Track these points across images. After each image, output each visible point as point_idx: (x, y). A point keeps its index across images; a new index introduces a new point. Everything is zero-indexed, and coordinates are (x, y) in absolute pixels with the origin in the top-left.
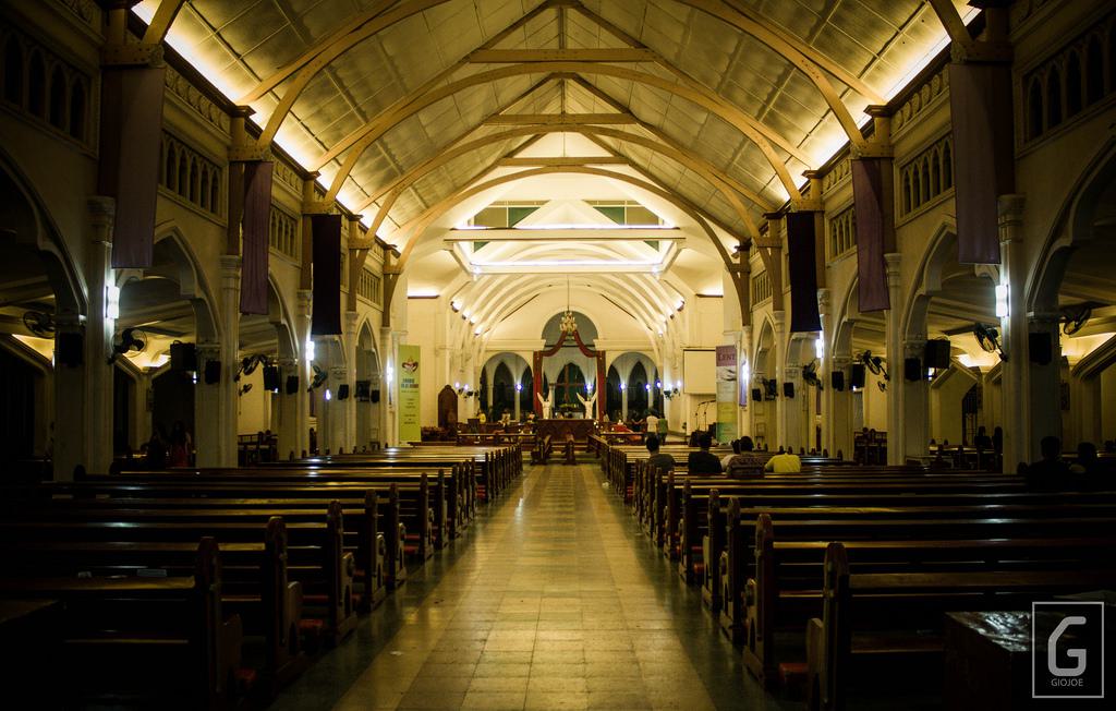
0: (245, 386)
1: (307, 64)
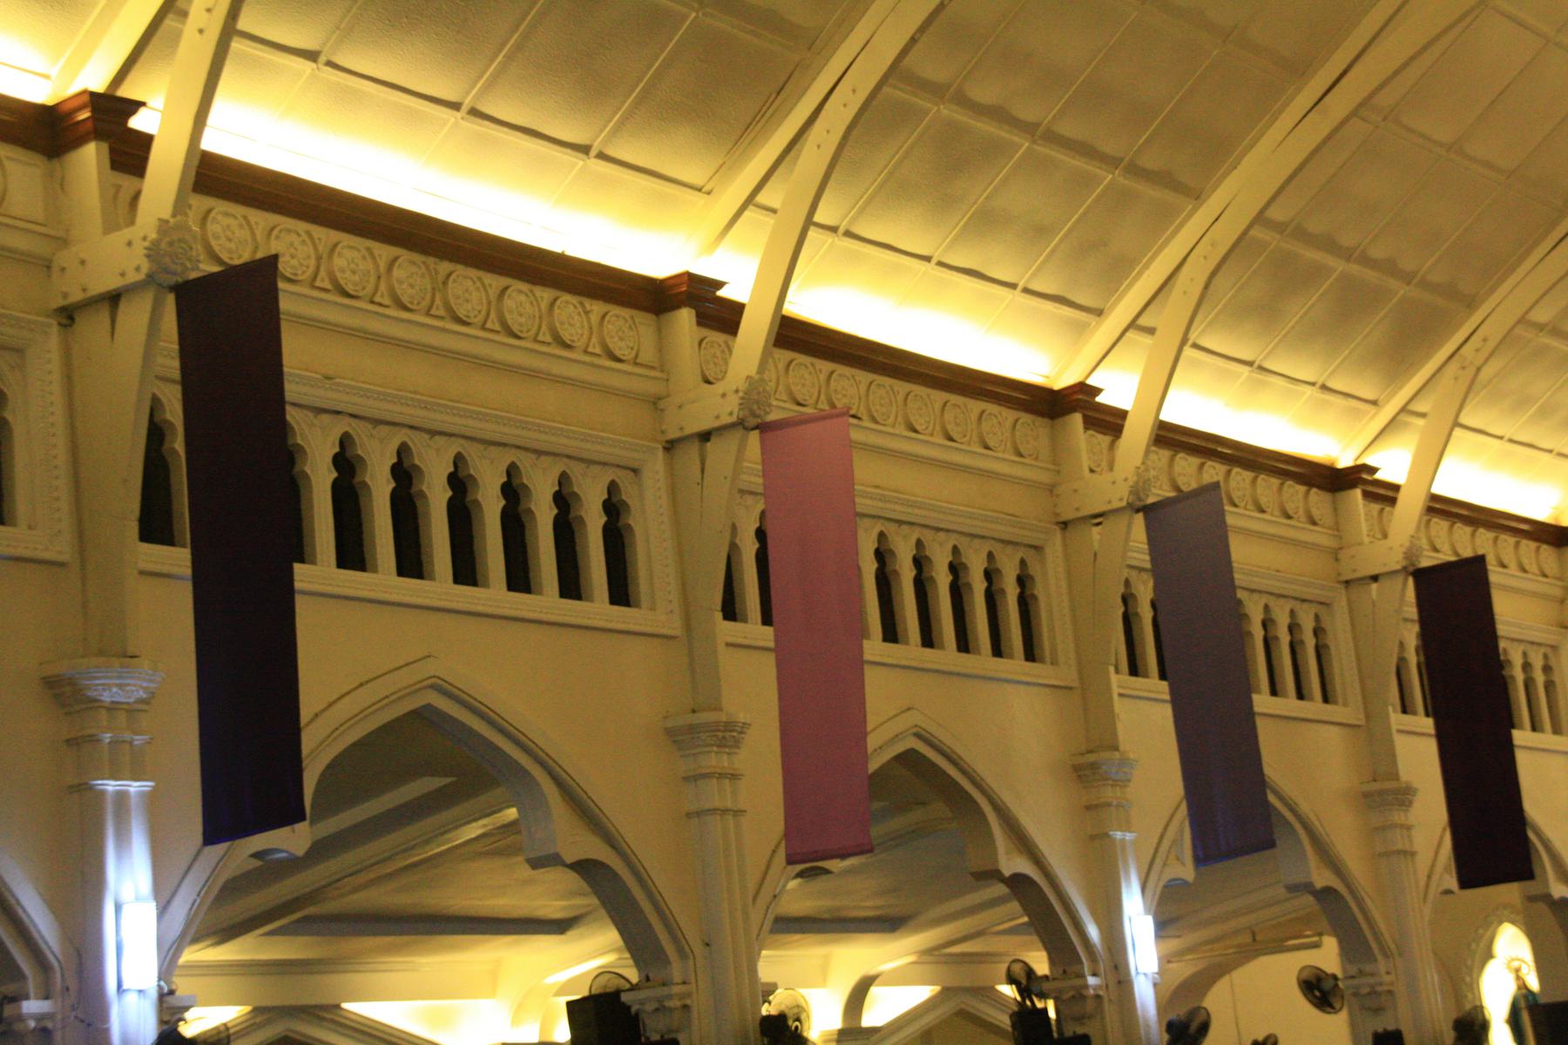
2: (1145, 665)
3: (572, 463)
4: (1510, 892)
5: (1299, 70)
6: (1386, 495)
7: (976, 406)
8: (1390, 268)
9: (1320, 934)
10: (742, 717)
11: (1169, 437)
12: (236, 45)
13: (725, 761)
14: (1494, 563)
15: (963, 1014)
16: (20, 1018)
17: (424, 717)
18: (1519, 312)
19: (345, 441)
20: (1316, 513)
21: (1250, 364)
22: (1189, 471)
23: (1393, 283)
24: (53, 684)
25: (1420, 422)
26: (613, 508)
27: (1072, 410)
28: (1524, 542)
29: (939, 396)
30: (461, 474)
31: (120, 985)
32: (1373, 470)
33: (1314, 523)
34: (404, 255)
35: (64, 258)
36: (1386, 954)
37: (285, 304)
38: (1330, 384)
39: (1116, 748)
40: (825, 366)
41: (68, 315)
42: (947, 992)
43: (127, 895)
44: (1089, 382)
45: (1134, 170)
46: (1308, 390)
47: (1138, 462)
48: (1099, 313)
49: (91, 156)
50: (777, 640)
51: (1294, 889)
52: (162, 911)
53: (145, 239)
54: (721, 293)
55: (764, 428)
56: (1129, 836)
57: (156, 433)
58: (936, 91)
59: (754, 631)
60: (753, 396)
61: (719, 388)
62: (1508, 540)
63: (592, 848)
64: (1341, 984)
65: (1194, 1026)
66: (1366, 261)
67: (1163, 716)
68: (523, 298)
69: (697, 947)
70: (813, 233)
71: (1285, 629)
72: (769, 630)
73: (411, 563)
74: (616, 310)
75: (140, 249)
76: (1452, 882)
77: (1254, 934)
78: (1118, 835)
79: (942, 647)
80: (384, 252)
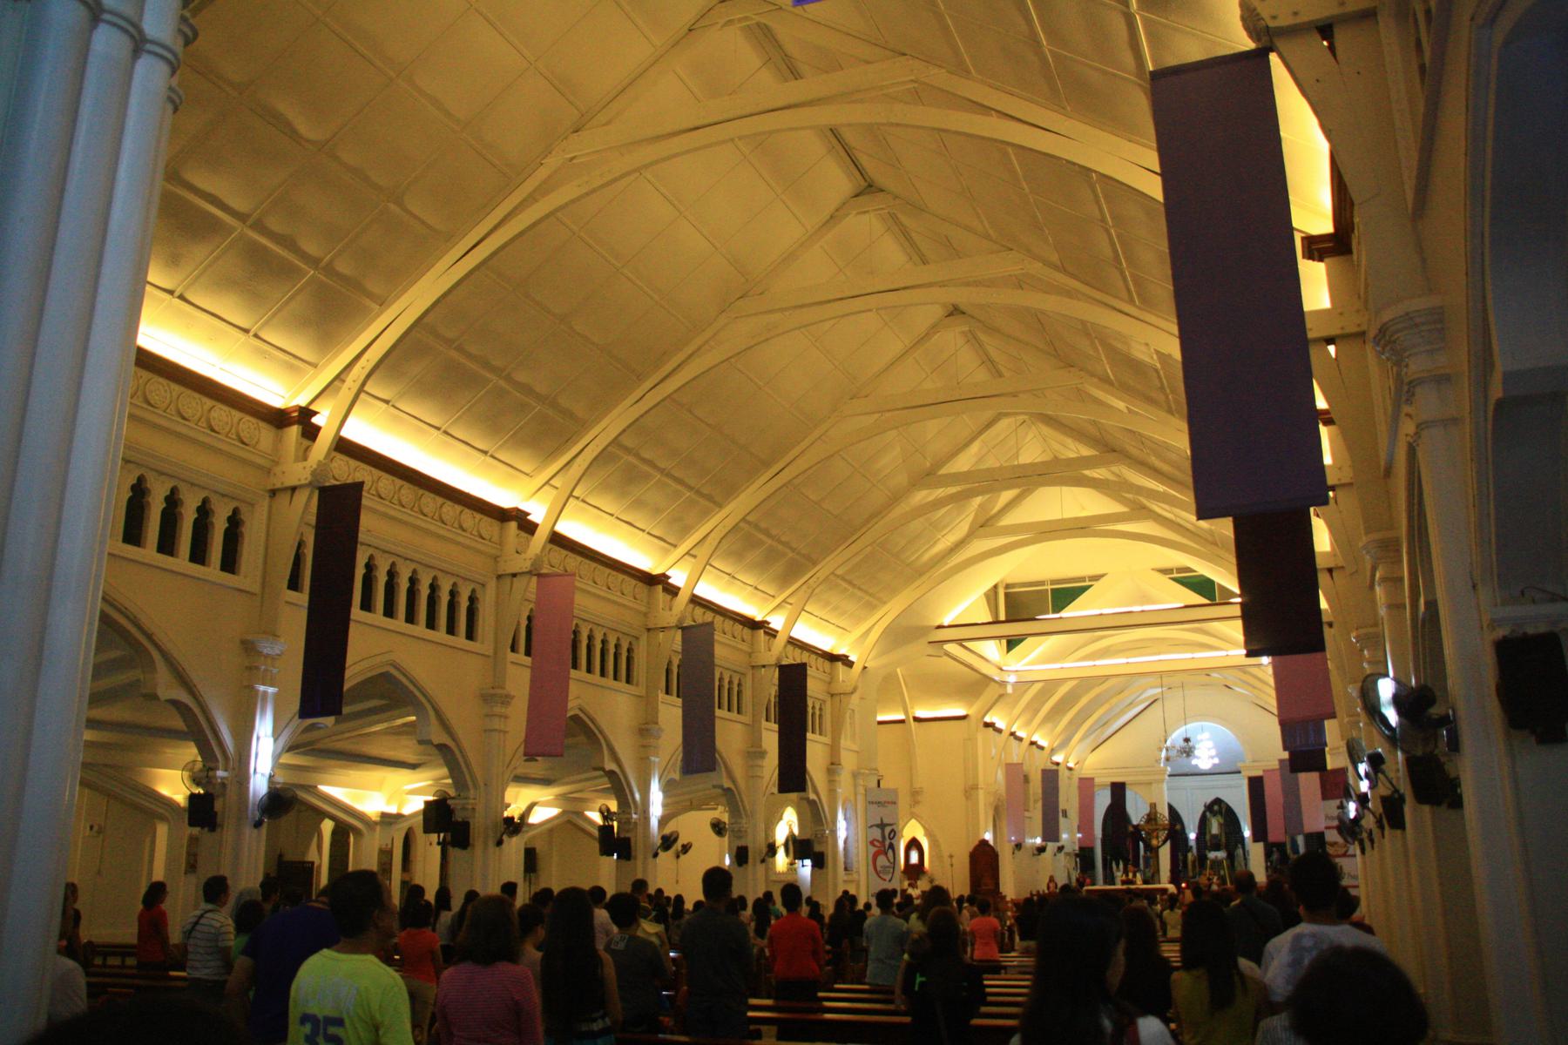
0: (684, 846)
1: (583, 450)
2: (303, 585)
3: (399, 559)
4: (794, 796)
5: (767, 464)
6: (772, 634)
7: (621, 576)
8: (787, 544)
9: (718, 805)
10: (512, 693)
11: (696, 601)
12: (363, 396)
13: (503, 710)
14: (547, 562)
15: (569, 822)
16: (215, 777)
17: (385, 676)
18: (832, 570)
19: (435, 578)
20: (745, 637)
21: (729, 575)
22: (701, 616)
23: (787, 550)
24: (244, 642)
25: (789, 606)
26: (473, 599)
27: (659, 583)
28: (820, 658)
29: (608, 571)
30: (435, 584)
31: (255, 770)
32: (769, 623)
33: (743, 641)
34: (407, 485)
35: (278, 470)
36: (747, 816)
37: (364, 502)
38: (758, 587)
39: (657, 723)
40: (564, 552)
41: (273, 493)
42: (564, 813)
43: (262, 734)
44: (667, 573)
45: (698, 492)
46: (750, 588)
47: (780, 649)
48: (675, 546)
49: (294, 431)
50: (532, 663)
51: (714, 787)
52: (275, 740)
53: (311, 467)
54: (529, 517)
55: (539, 575)
56: (657, 760)
57: (300, 545)
58: (627, 450)
59: (521, 657)
60: (537, 561)
61: (523, 556)
62: (814, 656)
63: (443, 739)
64: (727, 826)
65: (672, 838)
66: (780, 542)
67: (678, 713)
68: (449, 508)
69: (482, 784)
70: (571, 499)
71: (600, 642)
72: (529, 659)
73: (389, 612)
74: (485, 518)
75: (308, 471)
76: (775, 790)
77: (691, 803)
78: (653, 759)
79: (594, 674)
80: (399, 482)
